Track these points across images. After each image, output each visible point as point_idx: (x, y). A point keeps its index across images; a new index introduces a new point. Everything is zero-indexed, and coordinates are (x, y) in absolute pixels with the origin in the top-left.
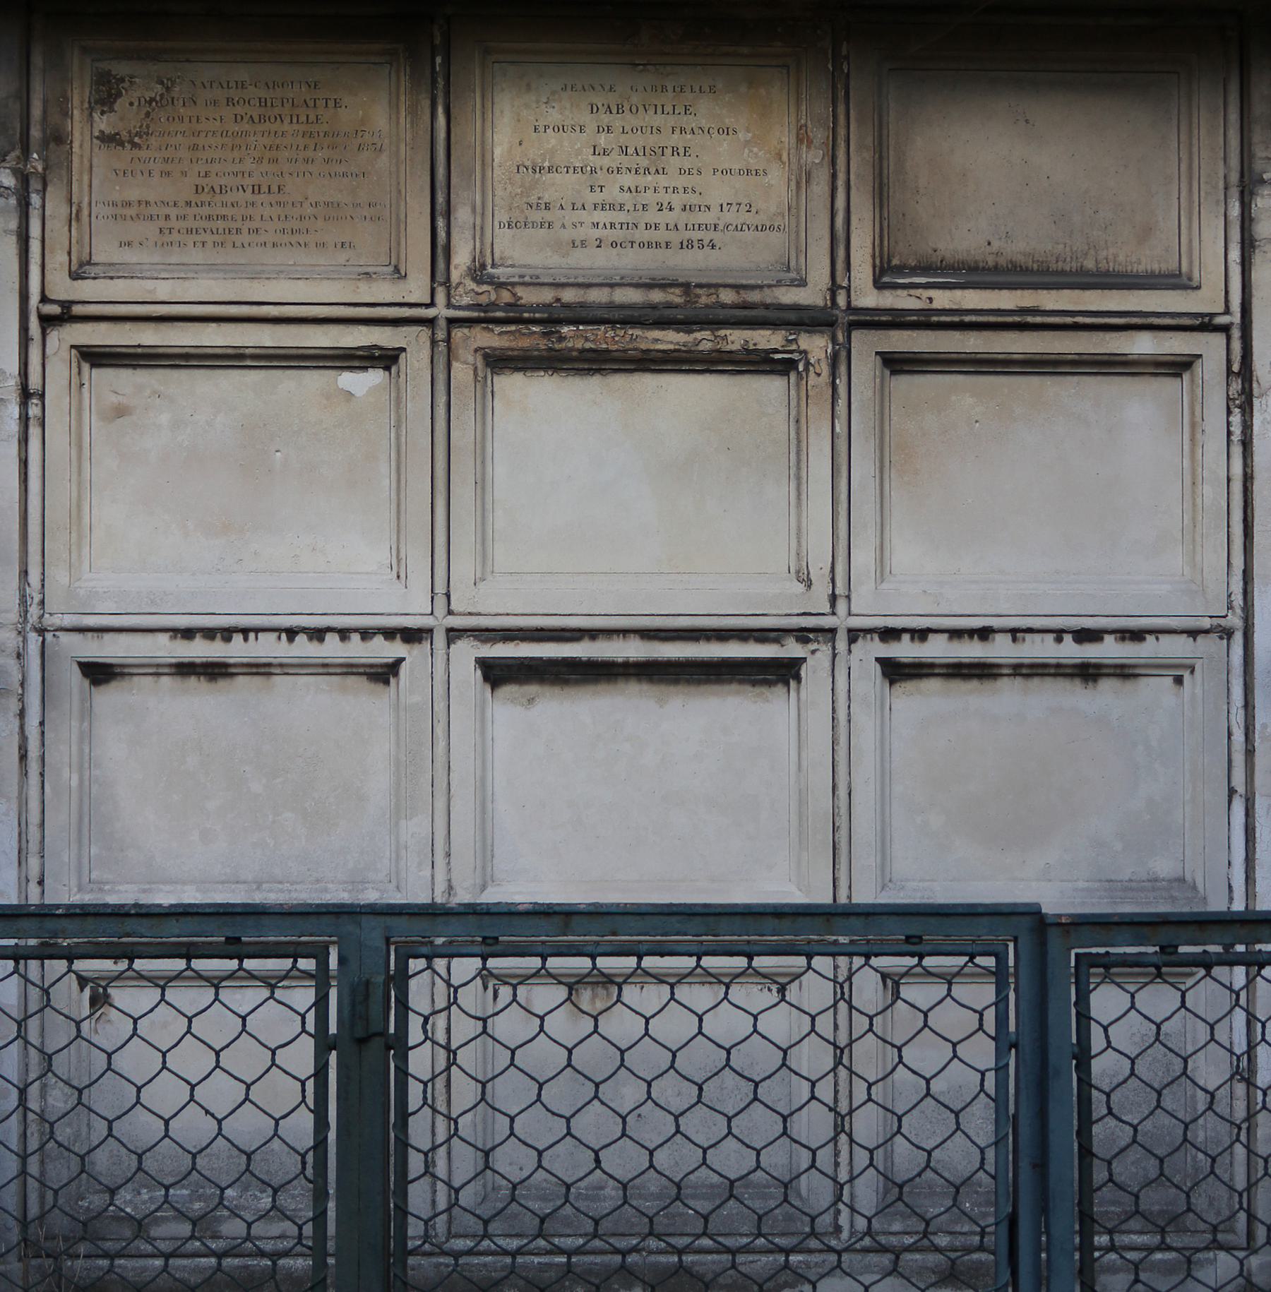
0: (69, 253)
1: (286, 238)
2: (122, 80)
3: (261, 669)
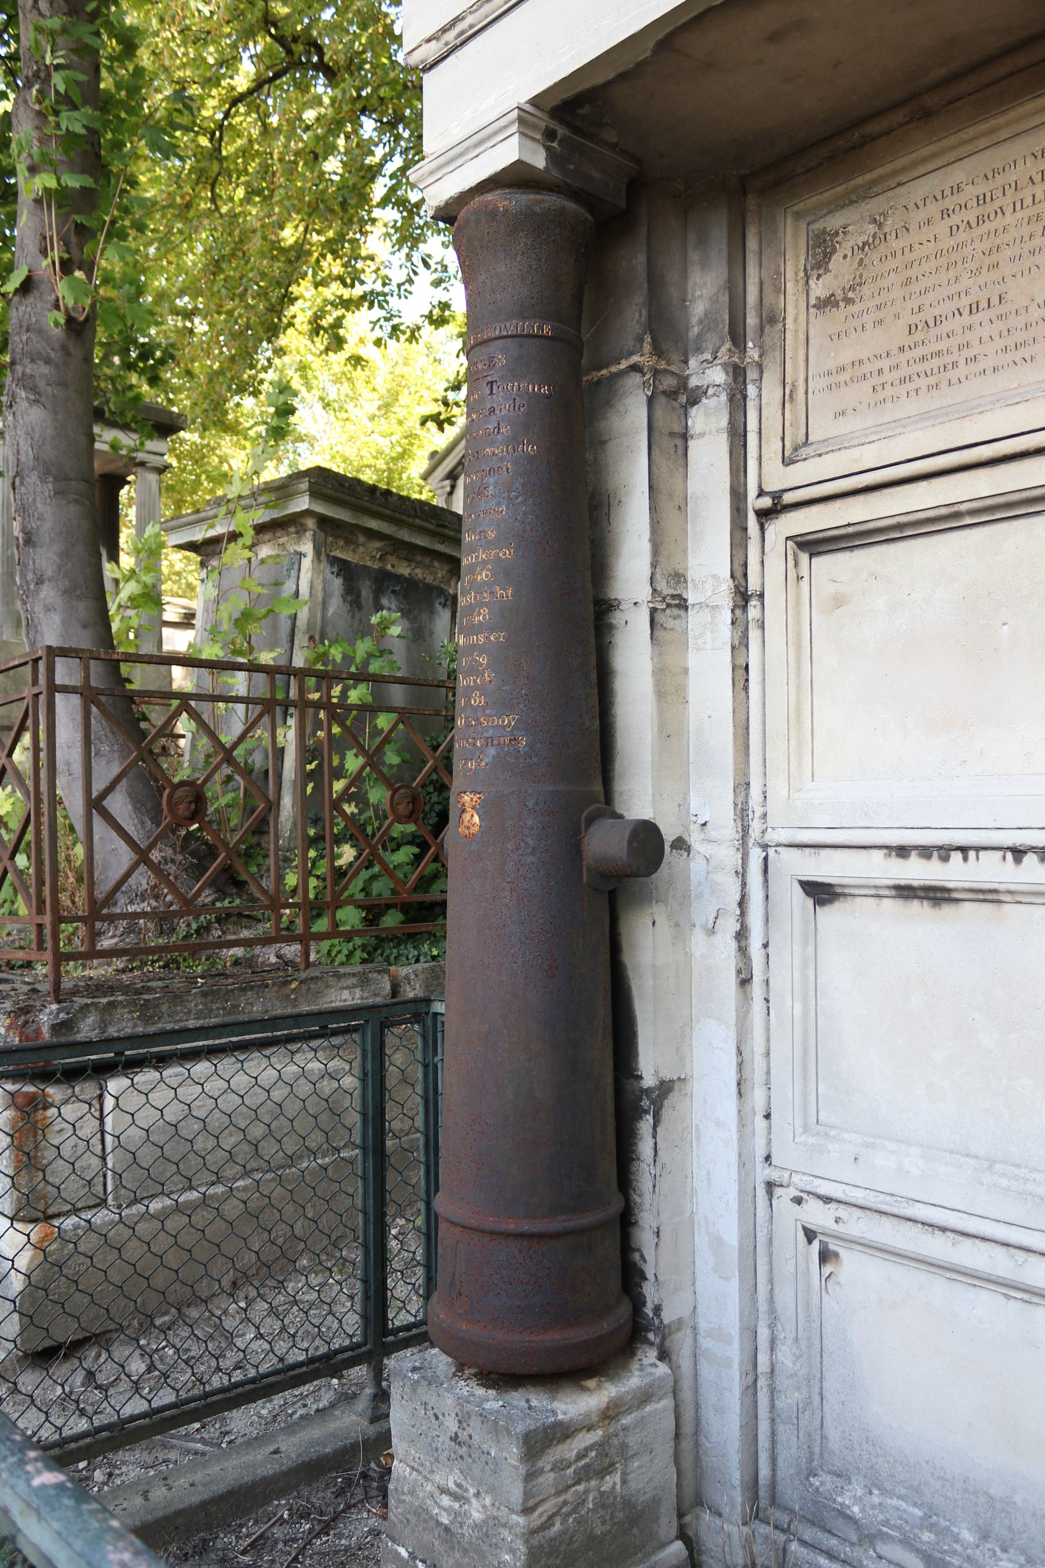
1: (1009, 357)
2: (837, 233)
3: (988, 896)
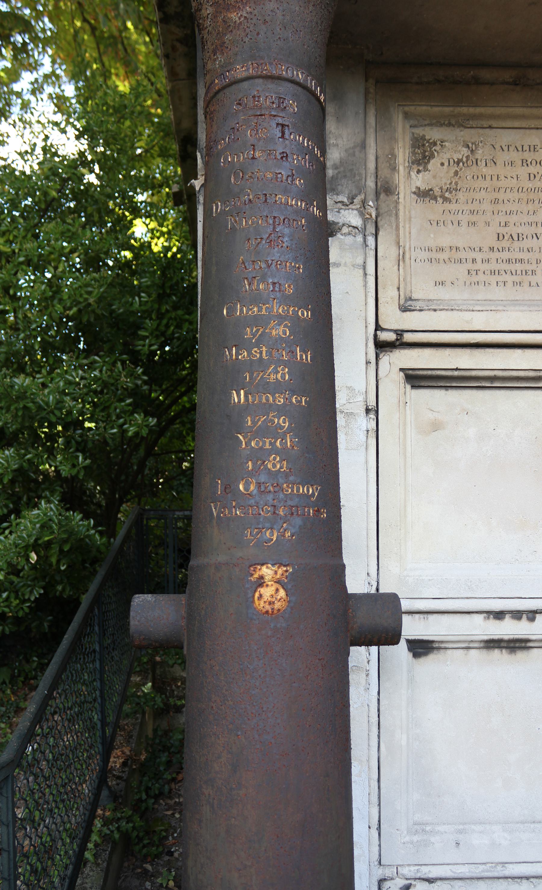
0: (399, 289)
2: (435, 144)
